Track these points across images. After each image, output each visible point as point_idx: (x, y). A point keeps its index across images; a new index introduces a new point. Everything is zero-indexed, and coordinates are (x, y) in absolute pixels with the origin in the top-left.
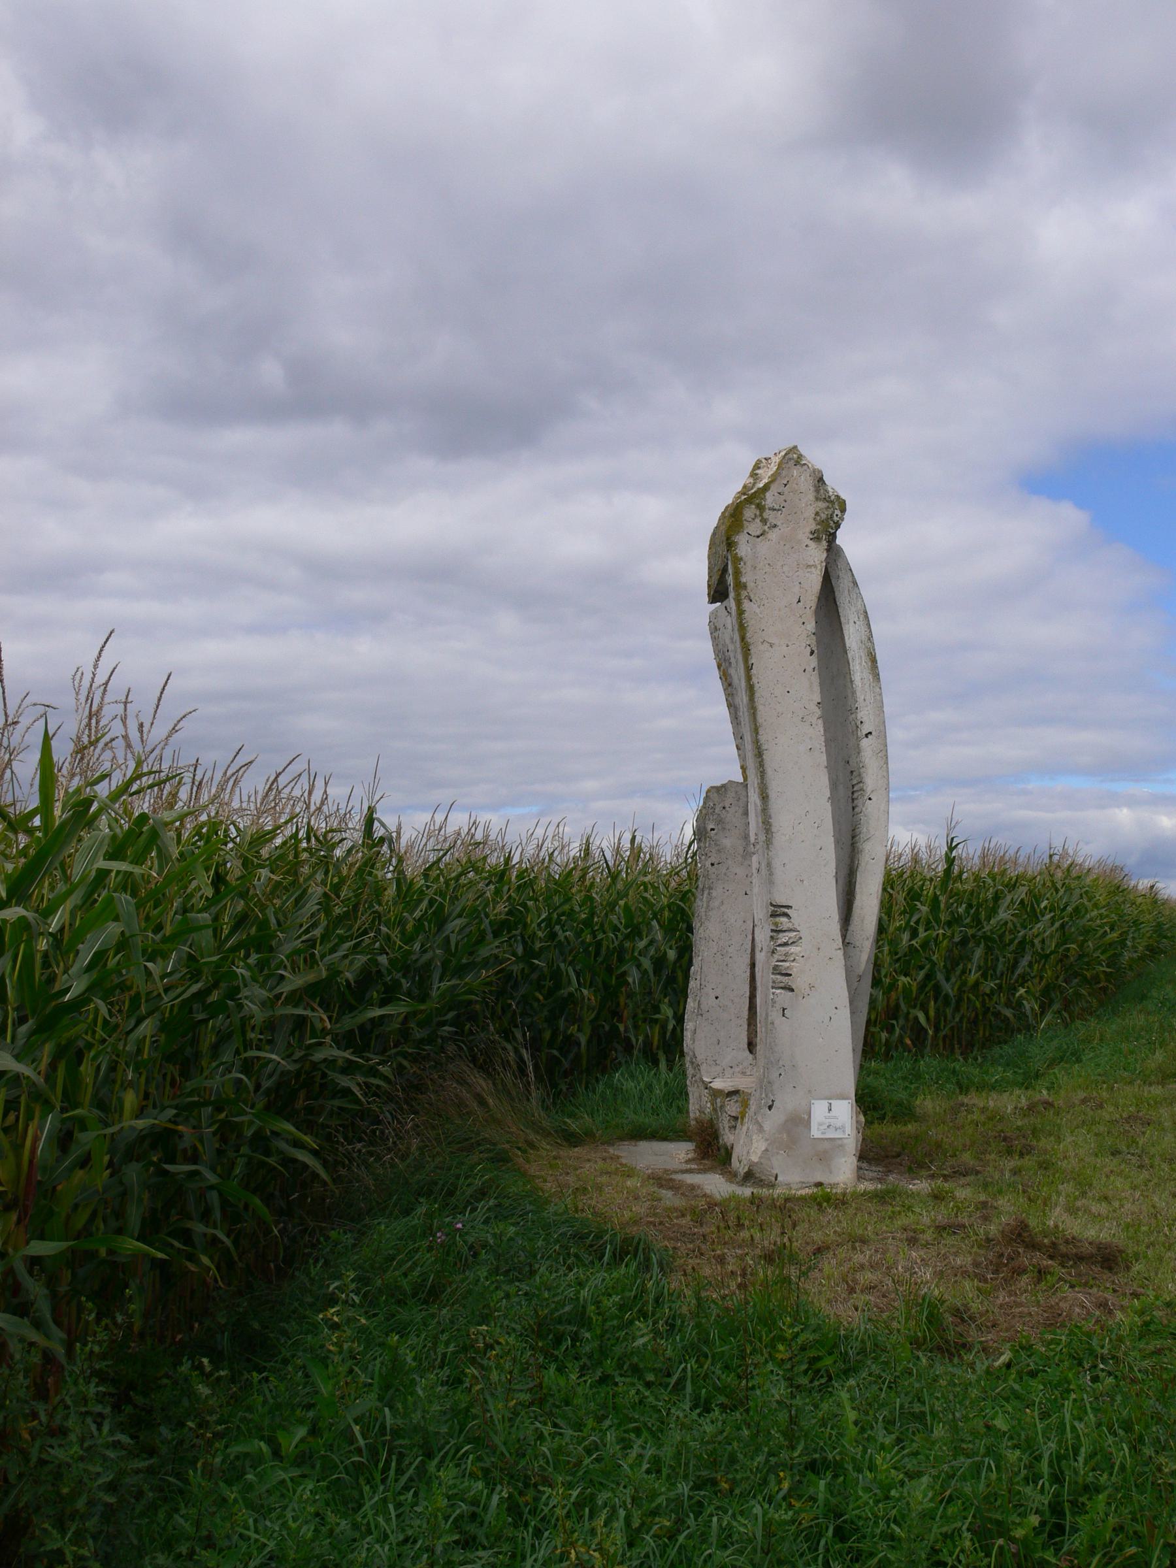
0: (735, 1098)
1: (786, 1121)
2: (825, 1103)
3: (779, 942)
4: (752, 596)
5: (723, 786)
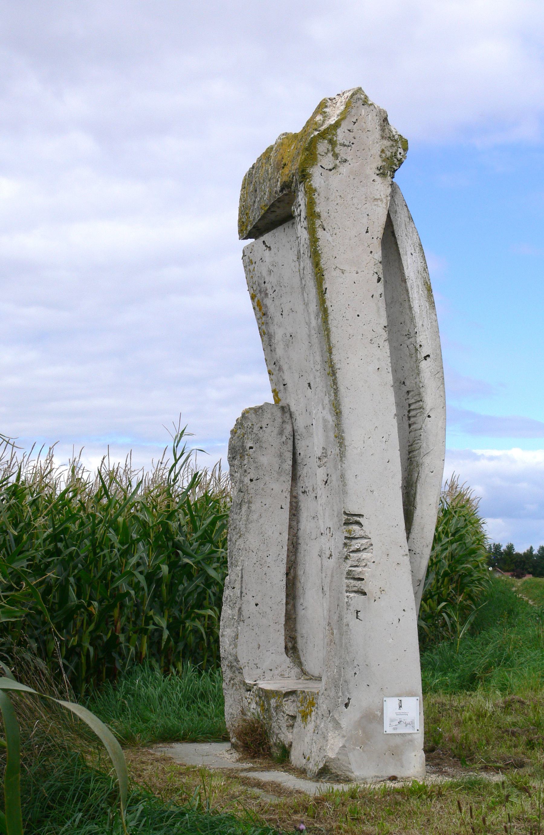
0: (292, 698)
1: (362, 718)
2: (396, 700)
3: (352, 548)
4: (325, 226)
5: (260, 408)
